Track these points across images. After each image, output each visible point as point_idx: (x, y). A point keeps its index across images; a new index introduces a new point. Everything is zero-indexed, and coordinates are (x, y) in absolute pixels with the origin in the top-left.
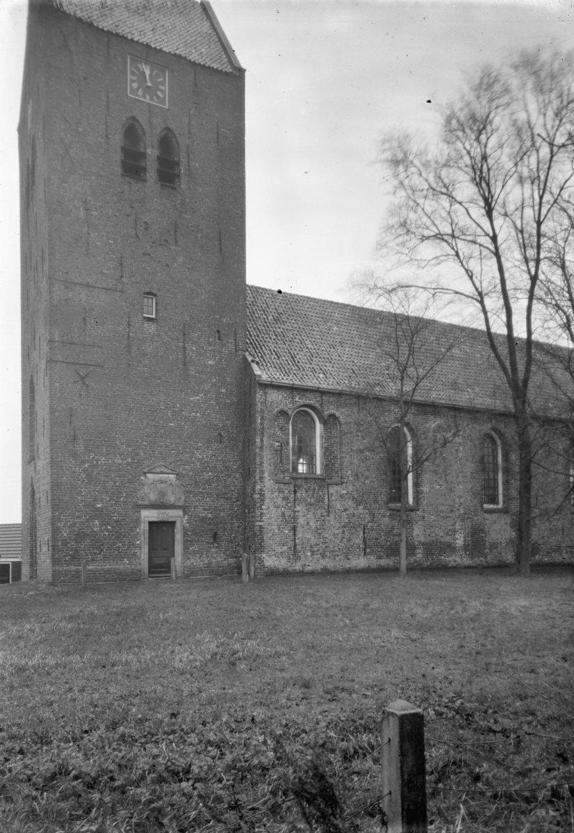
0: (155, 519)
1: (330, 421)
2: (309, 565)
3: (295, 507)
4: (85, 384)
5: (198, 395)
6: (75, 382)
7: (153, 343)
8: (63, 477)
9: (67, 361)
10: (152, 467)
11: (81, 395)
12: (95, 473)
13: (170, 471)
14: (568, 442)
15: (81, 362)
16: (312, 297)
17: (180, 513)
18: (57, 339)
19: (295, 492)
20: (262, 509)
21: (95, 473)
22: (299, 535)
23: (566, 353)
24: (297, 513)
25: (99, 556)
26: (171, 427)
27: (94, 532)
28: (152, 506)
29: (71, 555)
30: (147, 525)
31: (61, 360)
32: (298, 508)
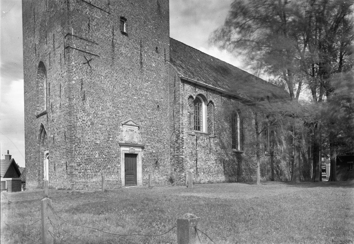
0: (128, 152)
1: (210, 104)
2: (203, 180)
3: (197, 148)
4: (90, 66)
5: (147, 83)
6: (84, 64)
7: (125, 48)
8: (77, 123)
9: (79, 49)
10: (126, 121)
11: (87, 72)
12: (96, 122)
13: (135, 124)
14: (334, 8)
15: (87, 51)
16: (170, 25)
17: (141, 150)
18: (73, 34)
19: (197, 140)
20: (183, 149)
21: (96, 122)
22: (198, 163)
23: (121, 147)
24: (197, 152)
25: (98, 173)
26: (135, 99)
27: (96, 158)
28: (126, 145)
29: (83, 173)
30: (137, 153)
31: (75, 48)
32: (198, 149)
